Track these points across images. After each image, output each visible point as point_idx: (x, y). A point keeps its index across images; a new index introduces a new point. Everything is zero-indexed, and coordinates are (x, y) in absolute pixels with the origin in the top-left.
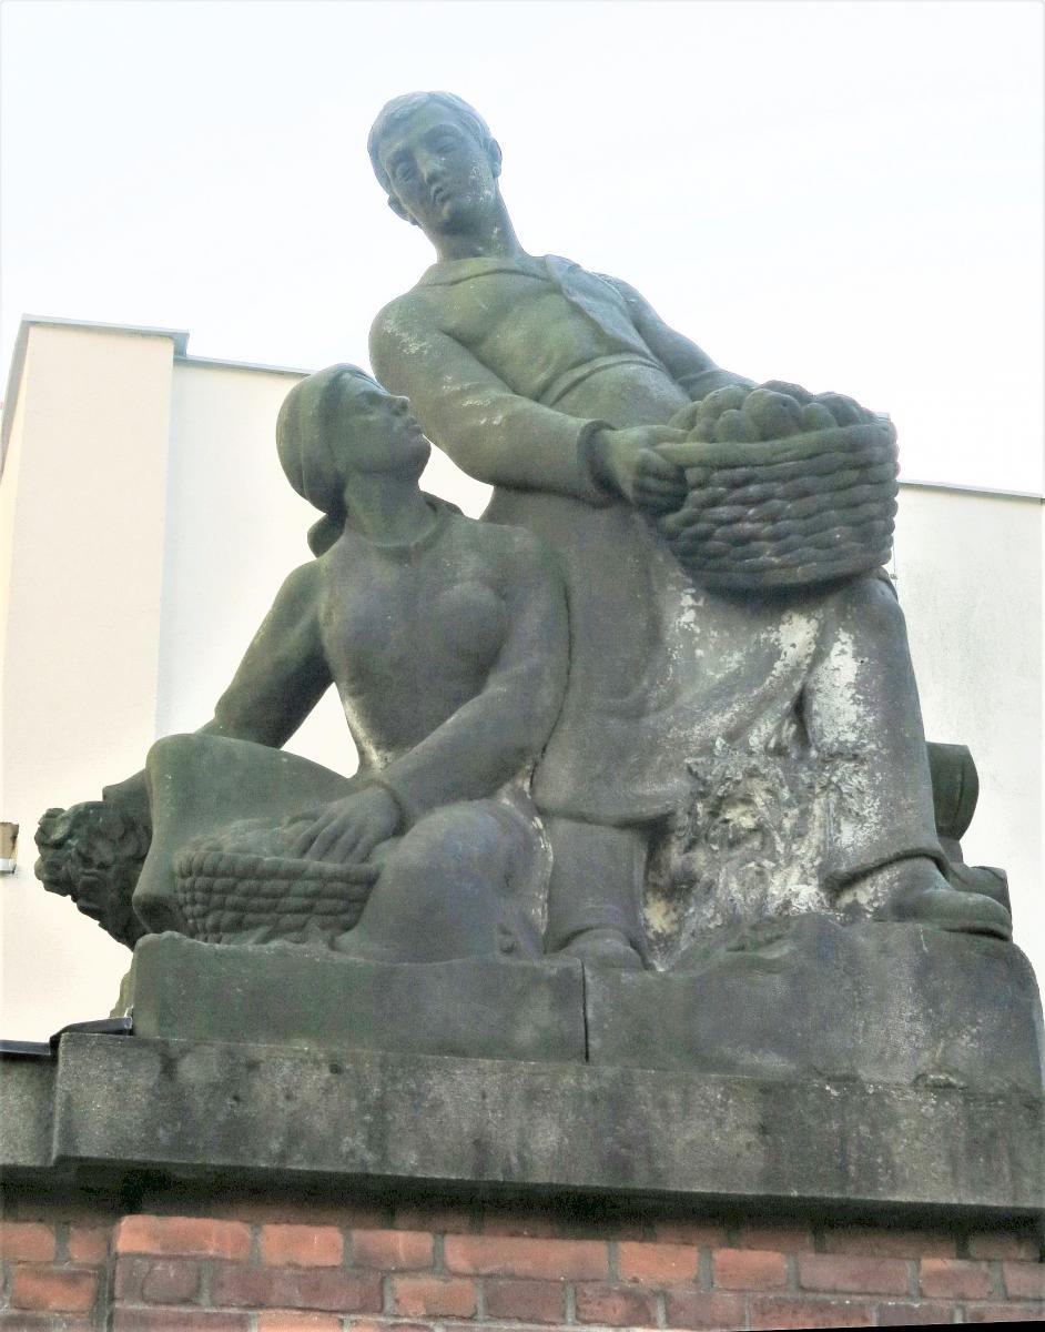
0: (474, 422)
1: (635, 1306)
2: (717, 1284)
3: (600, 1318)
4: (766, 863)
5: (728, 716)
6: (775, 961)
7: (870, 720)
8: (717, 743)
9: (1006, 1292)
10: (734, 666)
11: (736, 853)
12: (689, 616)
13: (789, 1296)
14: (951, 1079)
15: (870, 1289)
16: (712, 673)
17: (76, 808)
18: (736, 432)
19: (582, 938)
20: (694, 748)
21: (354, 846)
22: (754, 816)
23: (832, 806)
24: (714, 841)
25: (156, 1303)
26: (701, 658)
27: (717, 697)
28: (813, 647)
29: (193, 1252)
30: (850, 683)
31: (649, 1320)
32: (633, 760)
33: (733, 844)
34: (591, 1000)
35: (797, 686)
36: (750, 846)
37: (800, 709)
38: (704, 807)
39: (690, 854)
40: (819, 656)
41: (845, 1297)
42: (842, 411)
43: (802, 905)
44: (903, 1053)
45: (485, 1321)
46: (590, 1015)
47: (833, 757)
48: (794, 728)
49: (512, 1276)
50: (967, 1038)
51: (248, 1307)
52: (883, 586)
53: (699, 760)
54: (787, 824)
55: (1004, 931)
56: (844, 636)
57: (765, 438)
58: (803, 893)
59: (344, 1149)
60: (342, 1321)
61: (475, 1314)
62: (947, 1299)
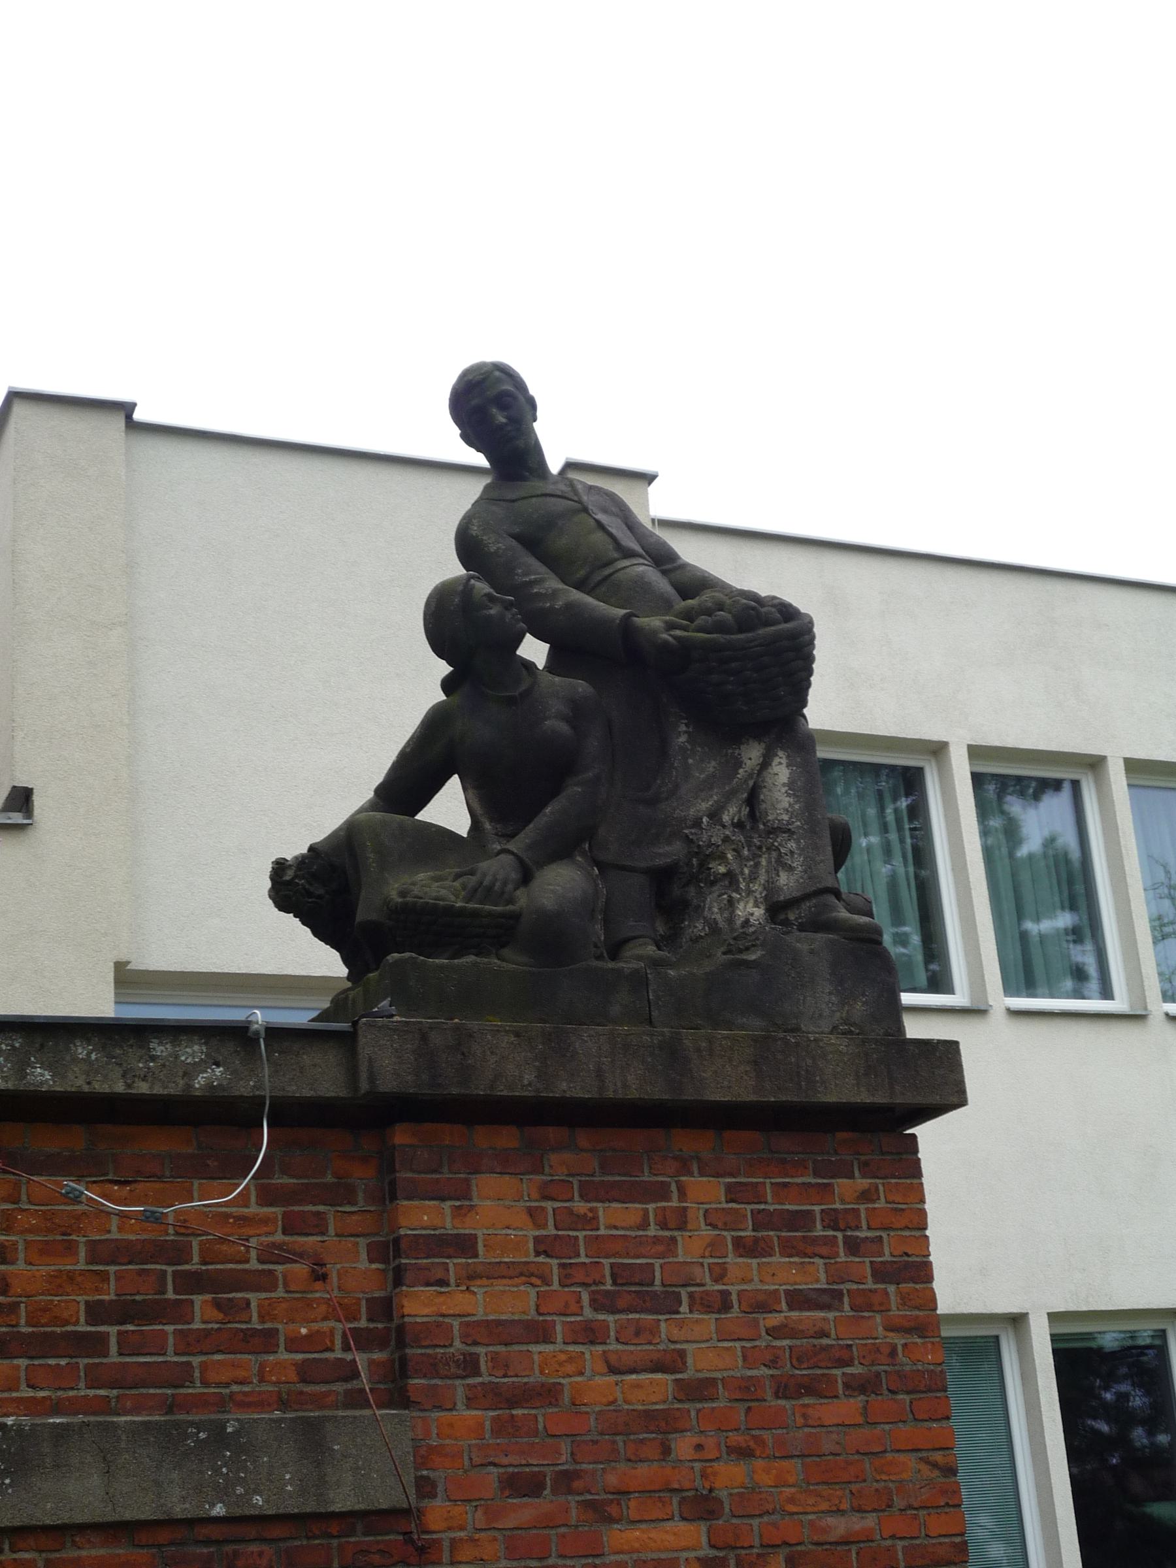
0: (541, 604)
4: (735, 895)
5: (710, 803)
6: (754, 961)
7: (797, 807)
8: (704, 820)
10: (711, 769)
12: (683, 739)
14: (852, 1028)
17: (296, 858)
18: (720, 627)
19: (631, 944)
20: (689, 823)
22: (726, 866)
23: (773, 860)
27: (702, 791)
28: (761, 759)
30: (784, 783)
33: (713, 883)
34: (651, 988)
35: (751, 783)
37: (753, 799)
40: (765, 764)
42: (787, 612)
44: (825, 1014)
45: (600, 1176)
47: (773, 831)
48: (748, 809)
51: (469, 1173)
52: (803, 720)
53: (693, 831)
55: (875, 937)
56: (781, 753)
57: (741, 631)
58: (751, 911)
59: (526, 1082)
60: (521, 1179)
61: (595, 1172)
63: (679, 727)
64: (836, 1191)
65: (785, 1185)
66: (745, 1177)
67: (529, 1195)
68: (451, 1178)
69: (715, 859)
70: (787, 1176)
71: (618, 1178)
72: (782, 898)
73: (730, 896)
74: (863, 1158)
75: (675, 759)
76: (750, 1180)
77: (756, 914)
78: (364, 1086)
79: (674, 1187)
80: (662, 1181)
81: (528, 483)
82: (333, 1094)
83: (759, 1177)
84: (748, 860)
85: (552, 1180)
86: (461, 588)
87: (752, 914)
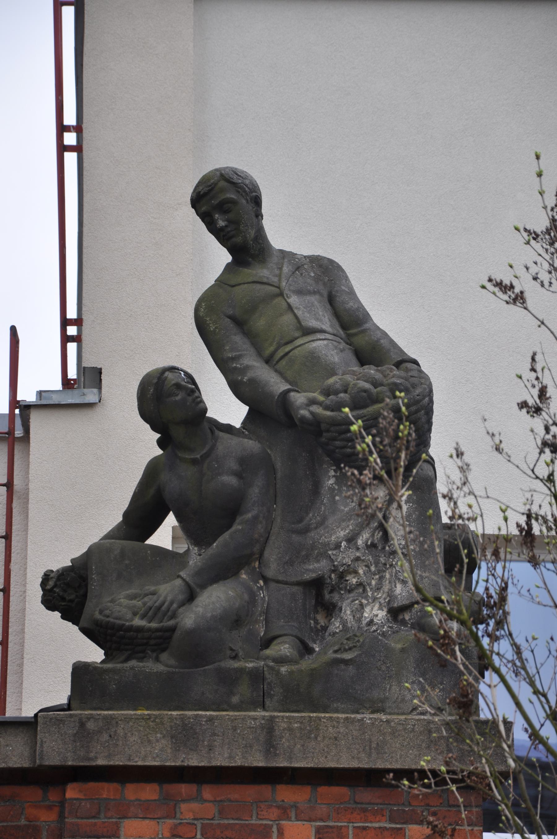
1: (282, 812)
2: (319, 801)
3: (267, 817)
4: (364, 601)
5: (347, 531)
8: (342, 544)
9: (449, 803)
11: (352, 595)
12: (332, 481)
13: (350, 806)
15: (386, 802)
16: (343, 508)
21: (168, 611)
24: (341, 589)
25: (82, 818)
26: (338, 500)
27: (344, 521)
28: (388, 498)
29: (97, 797)
31: (288, 817)
32: (304, 553)
33: (350, 591)
36: (358, 591)
38: (335, 575)
39: (331, 595)
41: (375, 806)
43: (379, 620)
44: (407, 698)
45: (218, 820)
46: (265, 689)
48: (381, 533)
49: (230, 801)
50: (437, 690)
51: (119, 818)
54: (373, 582)
61: (215, 817)
62: (422, 806)
63: (329, 472)
64: (407, 834)
65: (364, 828)
66: (332, 822)
67: (162, 834)
68: (105, 822)
69: (350, 573)
70: (366, 821)
71: (232, 822)
72: (395, 605)
73: (360, 602)
74: (433, 809)
75: (325, 497)
76: (336, 824)
77: (380, 616)
78: (38, 762)
79: (275, 829)
80: (266, 824)
81: (246, 270)
82: (19, 766)
83: (345, 822)
84: (375, 574)
85: (180, 823)
86: (155, 381)
87: (377, 616)
